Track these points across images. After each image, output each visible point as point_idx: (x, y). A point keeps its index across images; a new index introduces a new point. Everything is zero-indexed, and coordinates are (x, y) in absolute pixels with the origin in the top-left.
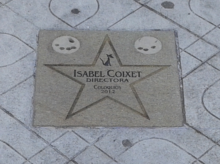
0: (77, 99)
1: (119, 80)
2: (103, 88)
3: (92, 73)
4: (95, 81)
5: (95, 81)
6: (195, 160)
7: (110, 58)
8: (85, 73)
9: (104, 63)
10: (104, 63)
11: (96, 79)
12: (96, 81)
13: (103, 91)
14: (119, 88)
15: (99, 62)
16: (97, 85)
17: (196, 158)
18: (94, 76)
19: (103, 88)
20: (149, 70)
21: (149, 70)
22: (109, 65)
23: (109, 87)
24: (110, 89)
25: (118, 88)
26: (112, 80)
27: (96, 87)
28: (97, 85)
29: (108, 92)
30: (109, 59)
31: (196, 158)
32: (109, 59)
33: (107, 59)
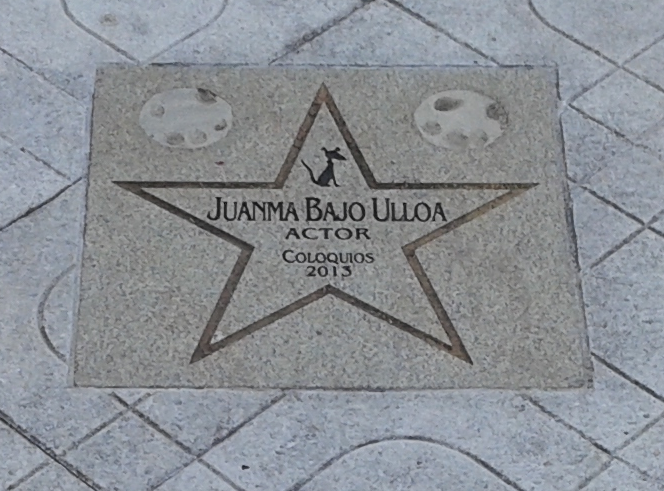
0: (375, 311)
1: (355, 234)
2: (313, 258)
3: (315, 206)
4: (358, 237)
5: (358, 237)
6: (122, 408)
7: (334, 161)
8: (329, 210)
9: (316, 179)
10: (316, 179)
11: (361, 231)
12: (362, 236)
13: (314, 268)
14: (366, 258)
15: (299, 174)
16: (292, 252)
17: (125, 404)
18: (390, 219)
19: (313, 258)
20: (474, 199)
21: (474, 199)
22: (331, 182)
23: (332, 258)
24: (336, 262)
25: (363, 259)
26: (331, 233)
27: (289, 256)
28: (292, 252)
29: (331, 272)
30: (330, 164)
31: (125, 404)
32: (330, 162)
33: (326, 165)
